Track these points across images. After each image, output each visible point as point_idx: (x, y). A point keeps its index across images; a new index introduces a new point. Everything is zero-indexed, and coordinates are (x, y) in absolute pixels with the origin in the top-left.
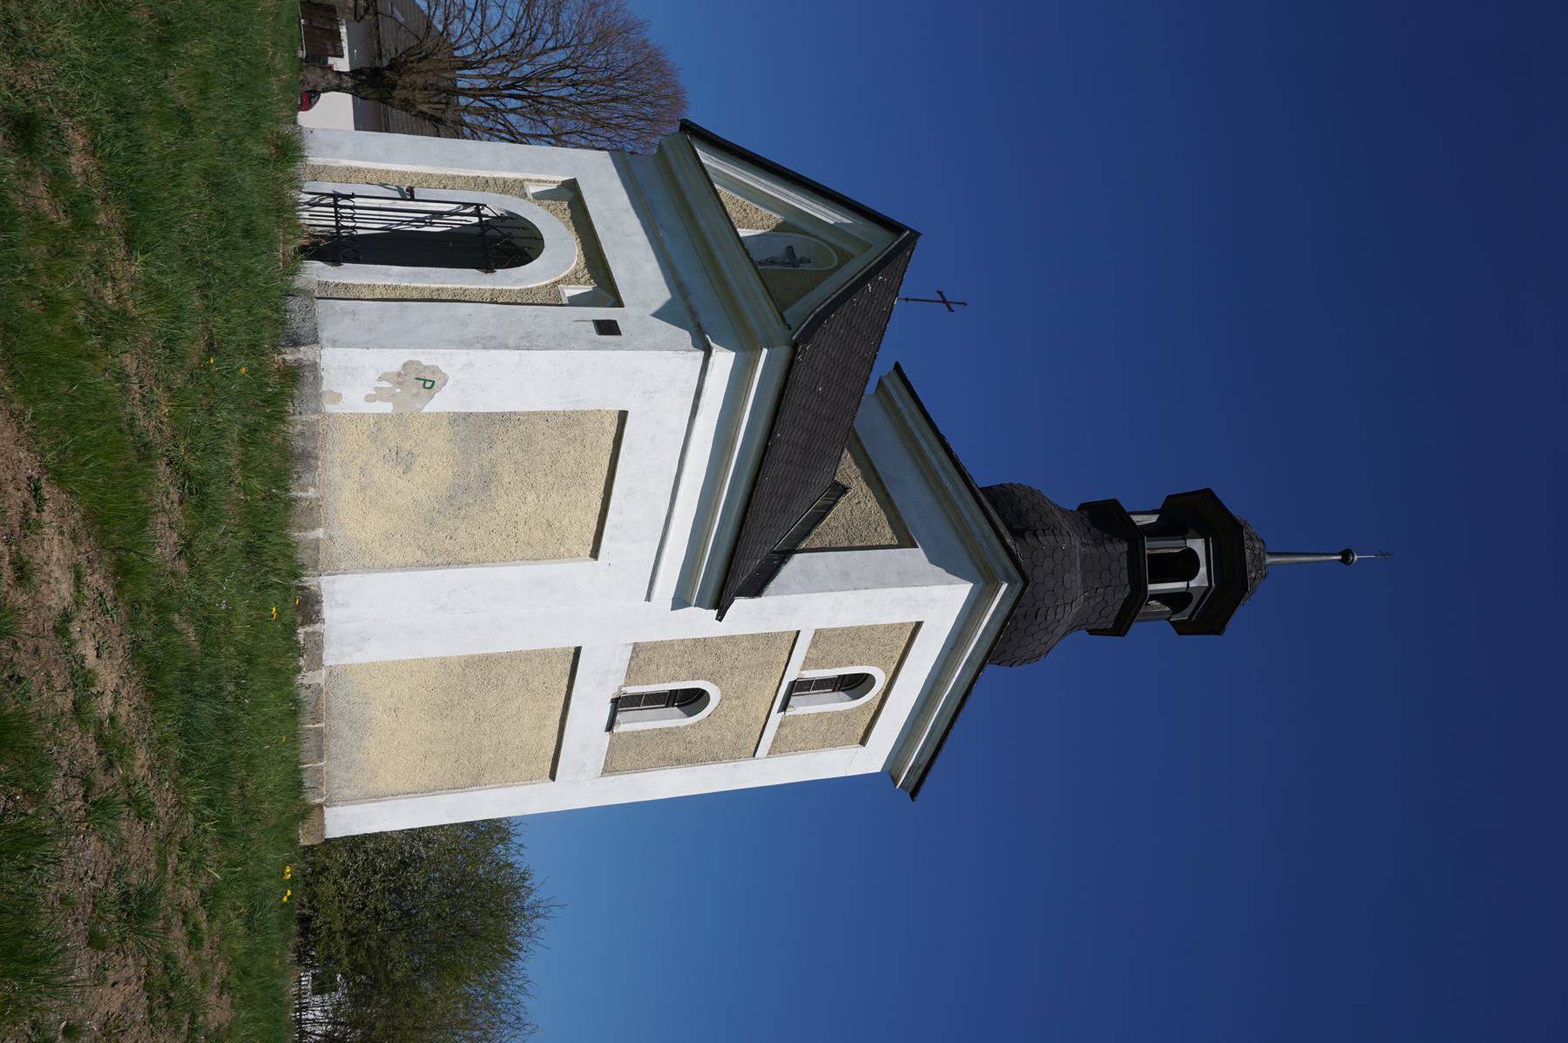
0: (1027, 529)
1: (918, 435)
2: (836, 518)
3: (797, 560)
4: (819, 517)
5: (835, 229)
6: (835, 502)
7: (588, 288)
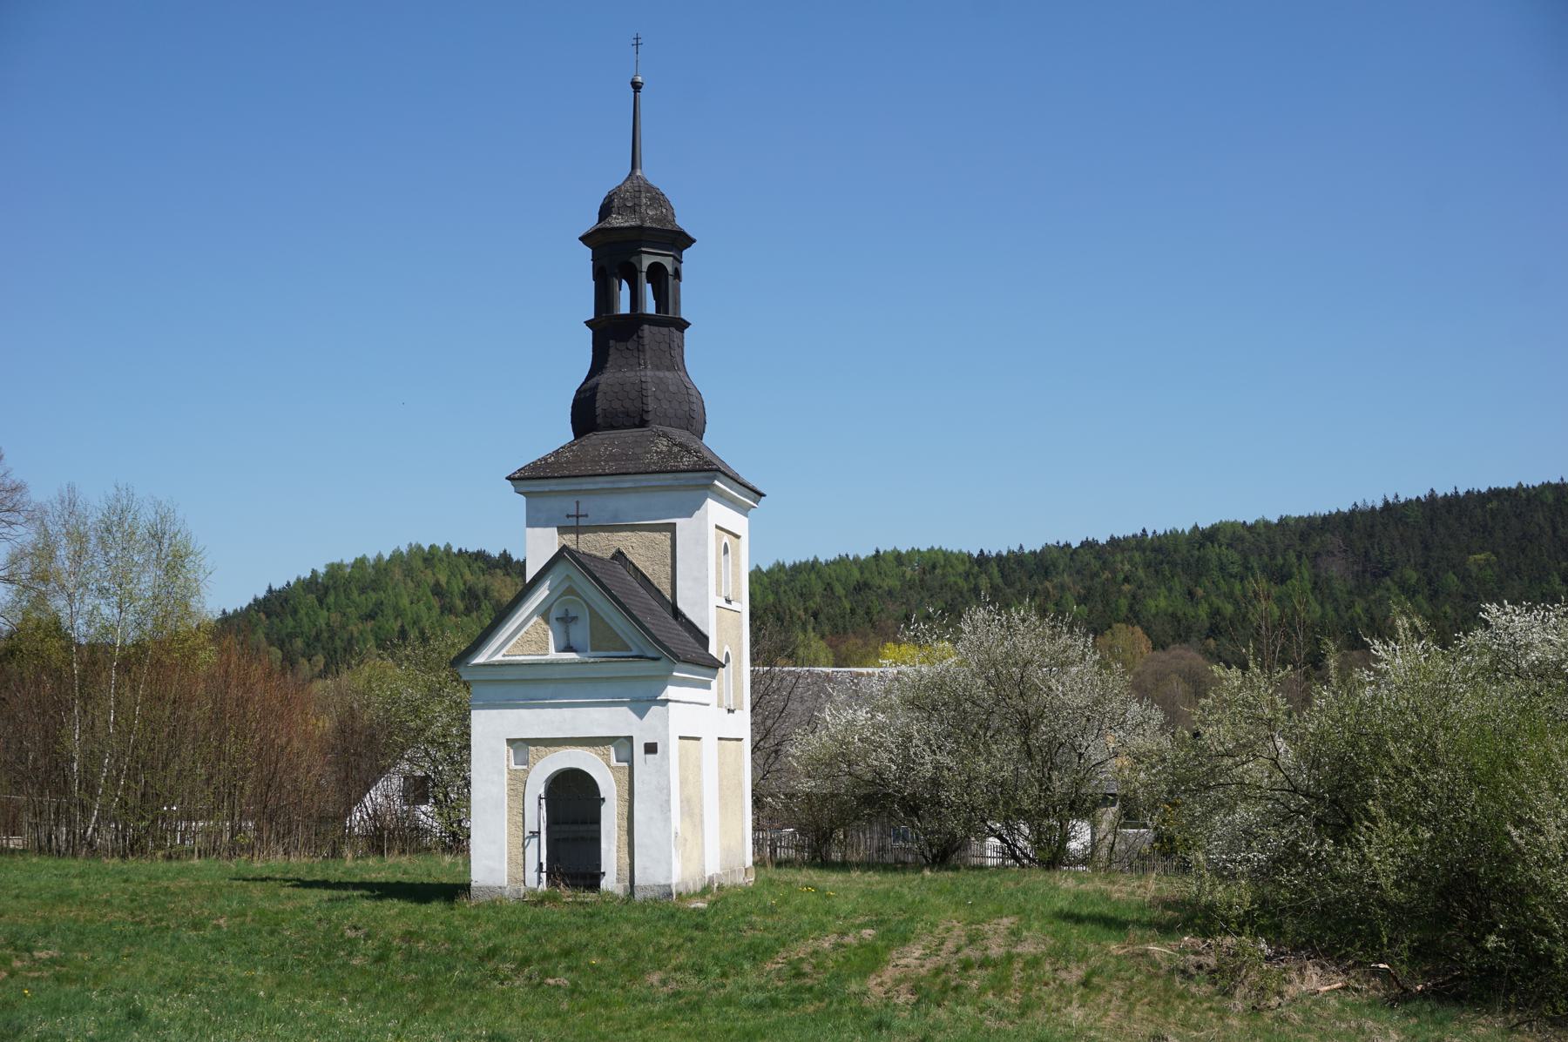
0: (642, 416)
1: (578, 487)
2: (645, 567)
3: (681, 605)
4: (645, 581)
5: (552, 591)
6: (631, 563)
7: (612, 749)
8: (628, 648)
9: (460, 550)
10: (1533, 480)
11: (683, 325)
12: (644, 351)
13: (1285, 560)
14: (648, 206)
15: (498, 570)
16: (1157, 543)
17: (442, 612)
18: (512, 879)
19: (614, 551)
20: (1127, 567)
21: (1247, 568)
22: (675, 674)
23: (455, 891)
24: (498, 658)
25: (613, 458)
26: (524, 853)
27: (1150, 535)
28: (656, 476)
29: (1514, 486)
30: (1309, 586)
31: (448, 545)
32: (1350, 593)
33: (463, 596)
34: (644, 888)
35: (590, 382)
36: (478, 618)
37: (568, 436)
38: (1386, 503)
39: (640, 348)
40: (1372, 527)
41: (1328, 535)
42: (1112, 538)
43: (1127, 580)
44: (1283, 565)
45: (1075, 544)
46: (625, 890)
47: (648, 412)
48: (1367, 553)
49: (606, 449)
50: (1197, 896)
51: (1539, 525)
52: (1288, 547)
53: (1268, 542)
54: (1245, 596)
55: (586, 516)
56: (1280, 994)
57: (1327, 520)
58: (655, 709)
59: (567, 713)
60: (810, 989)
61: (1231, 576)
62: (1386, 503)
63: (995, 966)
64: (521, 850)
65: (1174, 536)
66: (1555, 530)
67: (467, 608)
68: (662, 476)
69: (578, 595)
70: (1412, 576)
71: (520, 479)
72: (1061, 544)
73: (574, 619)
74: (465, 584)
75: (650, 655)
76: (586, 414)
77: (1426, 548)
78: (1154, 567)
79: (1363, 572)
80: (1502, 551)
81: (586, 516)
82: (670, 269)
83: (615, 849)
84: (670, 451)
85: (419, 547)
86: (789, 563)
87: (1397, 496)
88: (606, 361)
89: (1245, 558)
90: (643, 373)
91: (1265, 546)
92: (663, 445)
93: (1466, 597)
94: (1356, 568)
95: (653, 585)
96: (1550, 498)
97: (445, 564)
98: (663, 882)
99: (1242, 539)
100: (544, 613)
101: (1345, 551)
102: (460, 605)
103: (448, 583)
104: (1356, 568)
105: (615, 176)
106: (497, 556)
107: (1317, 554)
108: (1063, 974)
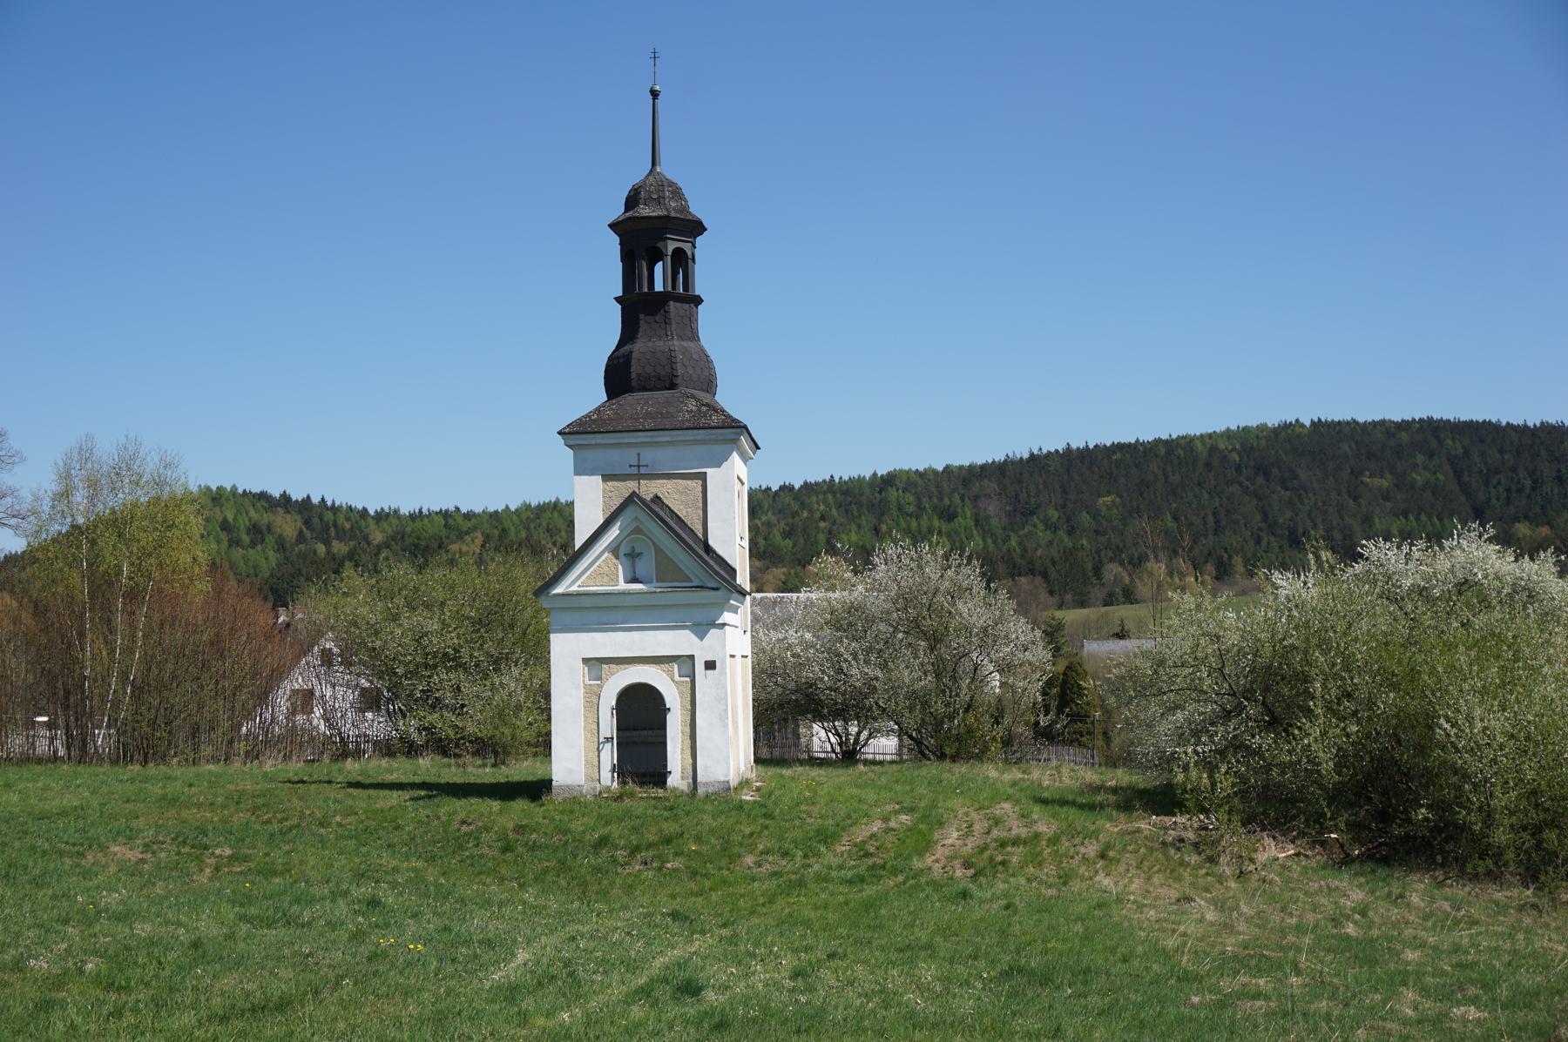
5: (622, 531)
6: (667, 506)
7: (676, 666)
8: (689, 579)
9: (245, 491)
10: (1148, 437)
11: (698, 301)
12: (670, 324)
13: (951, 501)
14: (670, 199)
15: (279, 509)
16: (845, 488)
17: (230, 546)
18: (589, 778)
19: (651, 496)
20: (822, 507)
21: (920, 508)
22: (732, 602)
23: (539, 789)
24: (574, 588)
25: (648, 415)
26: (599, 756)
27: (837, 480)
28: (690, 432)
29: (1133, 441)
30: (973, 524)
31: (234, 486)
32: (1004, 529)
33: (248, 532)
34: (706, 784)
35: (622, 350)
36: (263, 550)
38: (1032, 455)
39: (667, 321)
40: (1021, 474)
41: (986, 481)
42: (806, 483)
43: (823, 518)
44: (950, 506)
45: (775, 488)
46: (689, 784)
47: (677, 376)
48: (1017, 495)
49: (642, 408)
51: (1153, 473)
52: (953, 491)
53: (937, 487)
54: (920, 532)
55: (647, 466)
56: (1252, 860)
57: (984, 467)
58: (713, 631)
59: (636, 636)
60: (883, 867)
61: (908, 515)
62: (1032, 455)
63: (1025, 843)
64: (596, 753)
65: (860, 481)
66: (1166, 477)
67: (252, 541)
68: (696, 432)
69: (645, 535)
70: (1054, 514)
71: (569, 433)
72: (763, 488)
73: (640, 554)
74: (250, 520)
75: (709, 585)
76: (618, 377)
77: (1065, 491)
78: (845, 508)
79: (1015, 511)
80: (1125, 494)
81: (647, 466)
82: (689, 253)
83: (679, 751)
84: (699, 410)
85: (208, 488)
86: (534, 503)
87: (1040, 449)
88: (637, 331)
89: (919, 499)
90: (671, 343)
91: (933, 489)
93: (1097, 532)
94: (1008, 508)
95: (687, 525)
96: (1162, 451)
97: (232, 503)
98: (722, 779)
99: (915, 484)
100: (614, 550)
101: (1000, 494)
102: (246, 539)
103: (235, 519)
104: (1008, 508)
105: (637, 172)
106: (278, 496)
107: (977, 498)
108: (1082, 850)
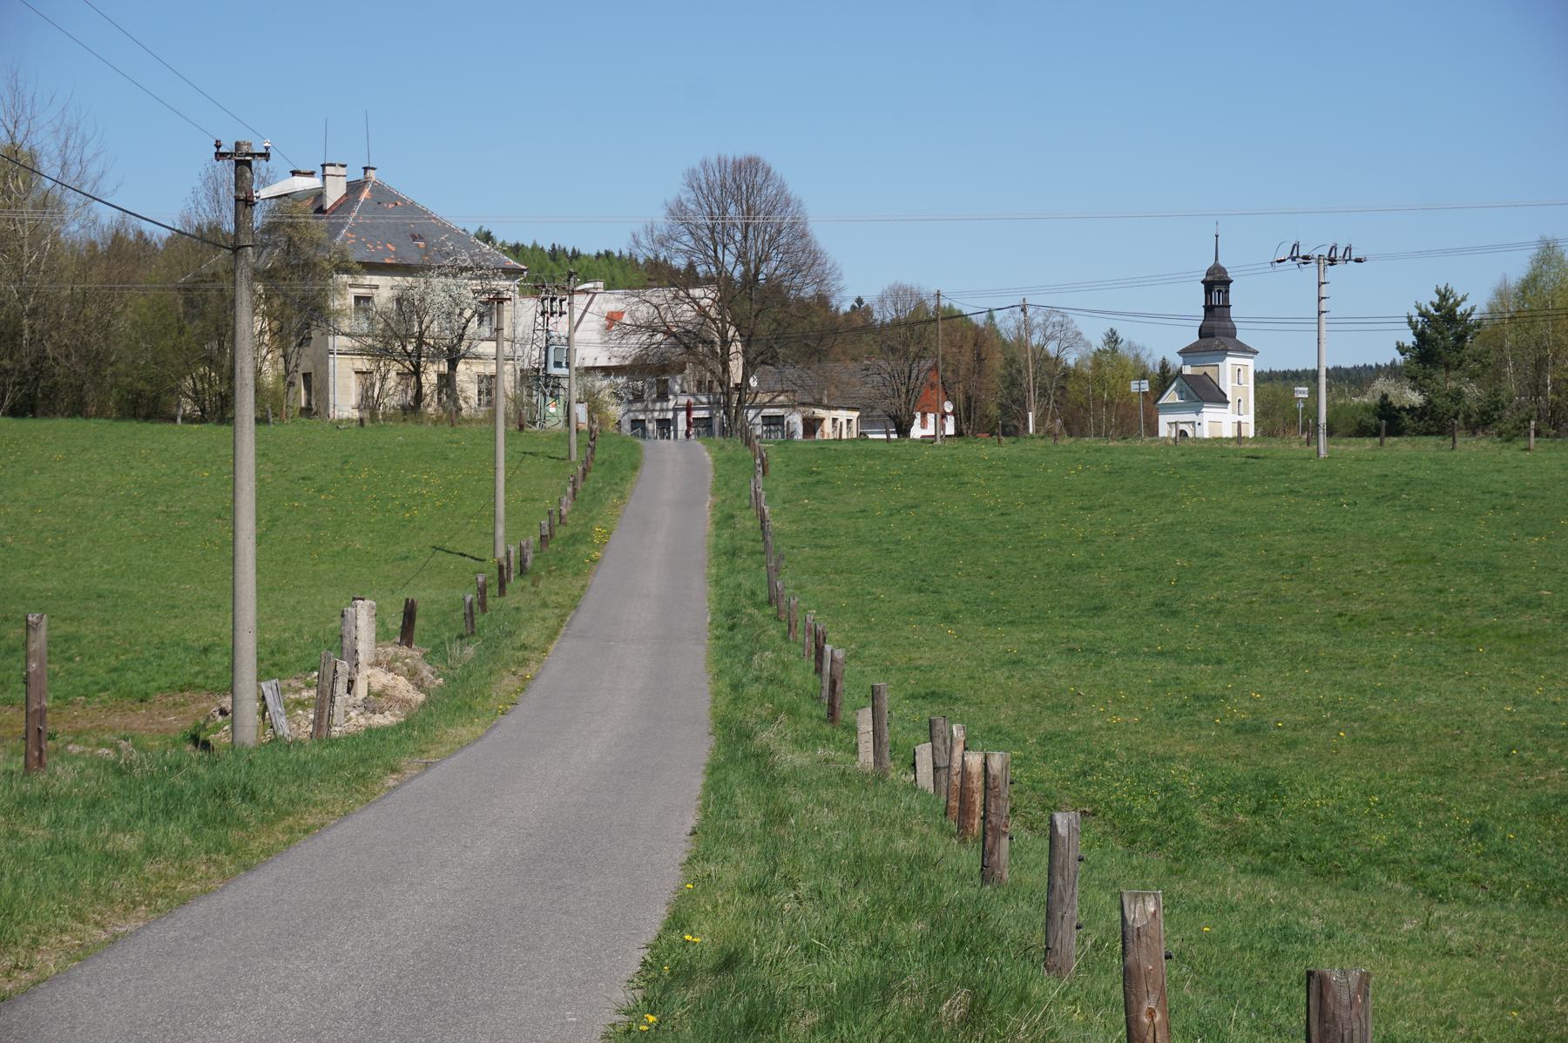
15: (281, 350)
37: (1198, 339)
50: (236, 236)
76: (1203, 333)
92: (1217, 342)
100: (1175, 389)
105: (1211, 263)
